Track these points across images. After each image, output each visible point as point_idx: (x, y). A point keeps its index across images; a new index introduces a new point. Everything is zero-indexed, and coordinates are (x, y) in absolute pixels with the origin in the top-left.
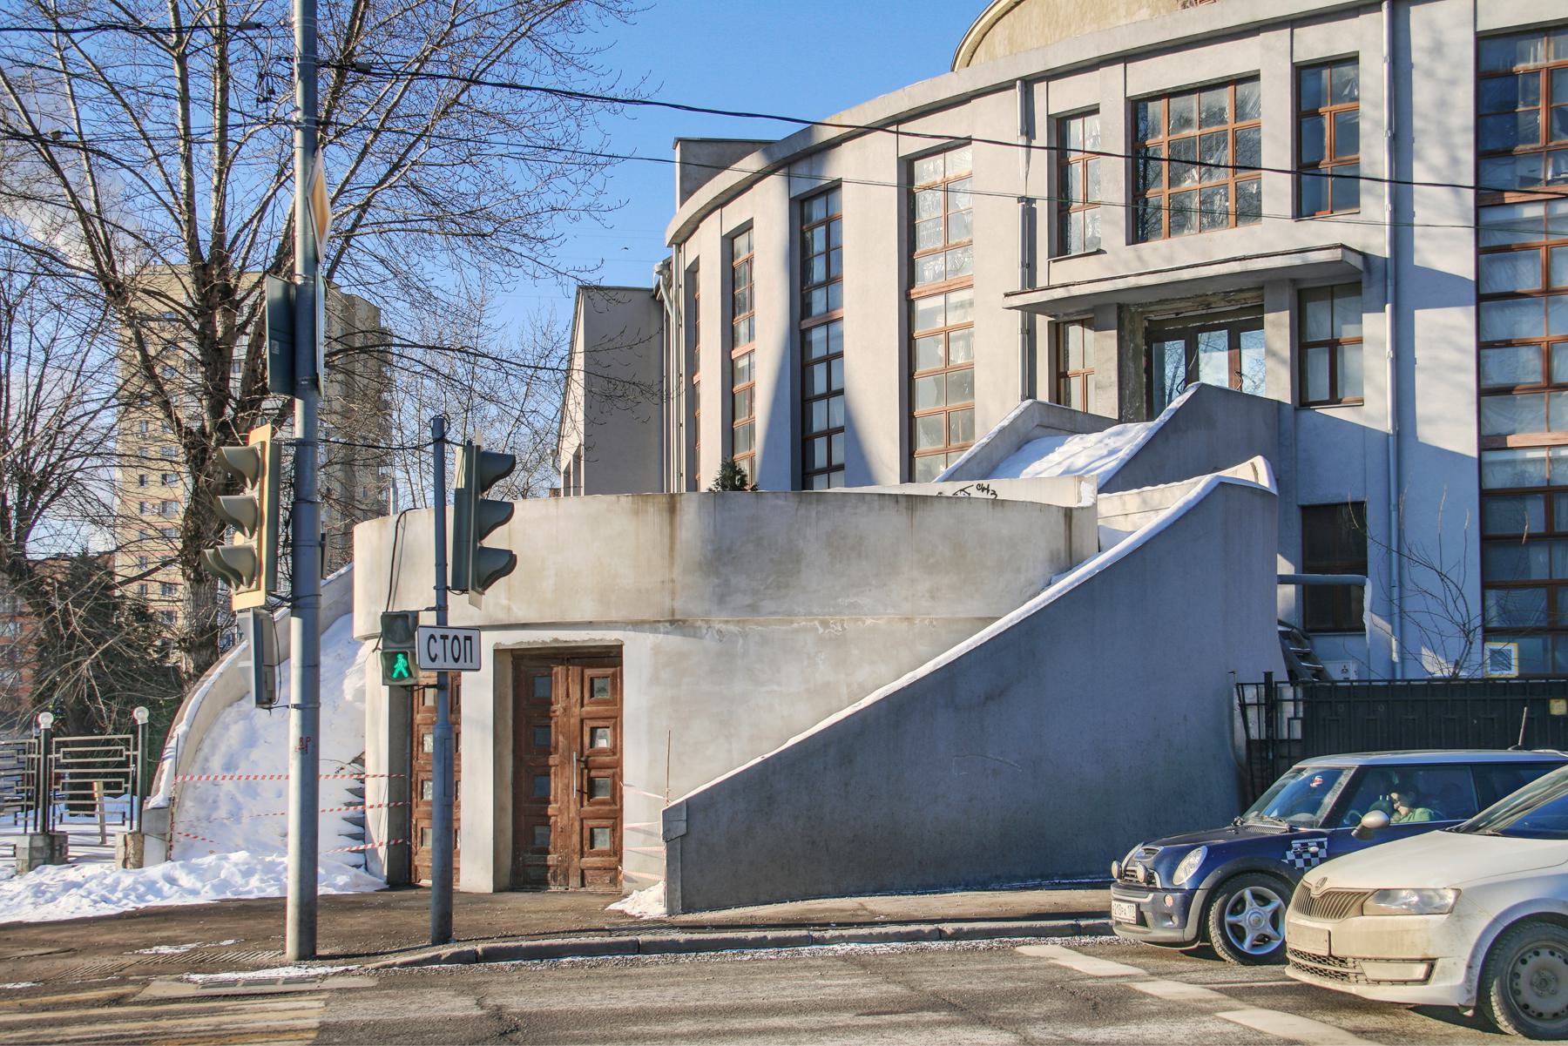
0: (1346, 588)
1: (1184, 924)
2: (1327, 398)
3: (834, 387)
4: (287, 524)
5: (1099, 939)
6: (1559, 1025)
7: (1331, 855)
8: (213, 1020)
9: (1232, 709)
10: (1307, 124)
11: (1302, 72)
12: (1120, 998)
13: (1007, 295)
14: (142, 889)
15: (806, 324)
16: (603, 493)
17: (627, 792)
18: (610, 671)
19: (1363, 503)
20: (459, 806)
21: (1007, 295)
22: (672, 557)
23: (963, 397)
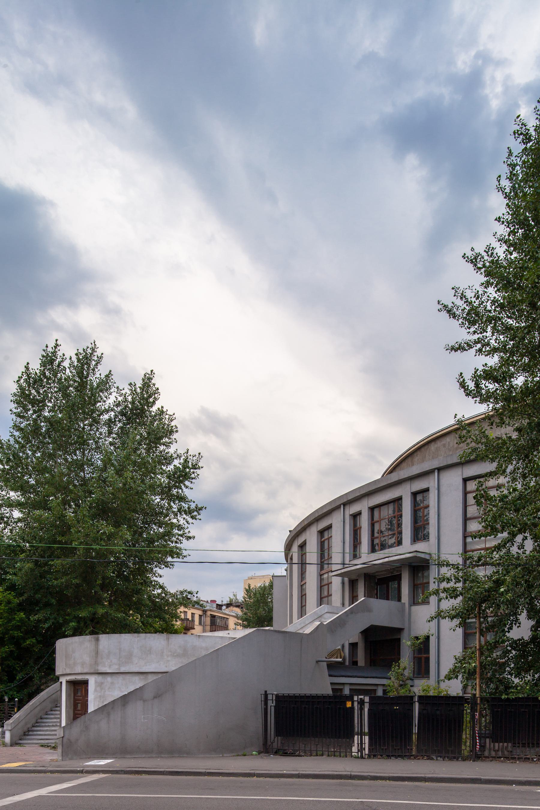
0: (459, 741)
3: (330, 594)
4: (470, 722)
5: (297, 773)
6: (539, 790)
7: (74, 635)
9: (27, 761)
10: (123, 772)
11: (415, 494)
14: (445, 563)
17: (68, 639)
18: (361, 662)
22: (391, 472)
23: (412, 704)
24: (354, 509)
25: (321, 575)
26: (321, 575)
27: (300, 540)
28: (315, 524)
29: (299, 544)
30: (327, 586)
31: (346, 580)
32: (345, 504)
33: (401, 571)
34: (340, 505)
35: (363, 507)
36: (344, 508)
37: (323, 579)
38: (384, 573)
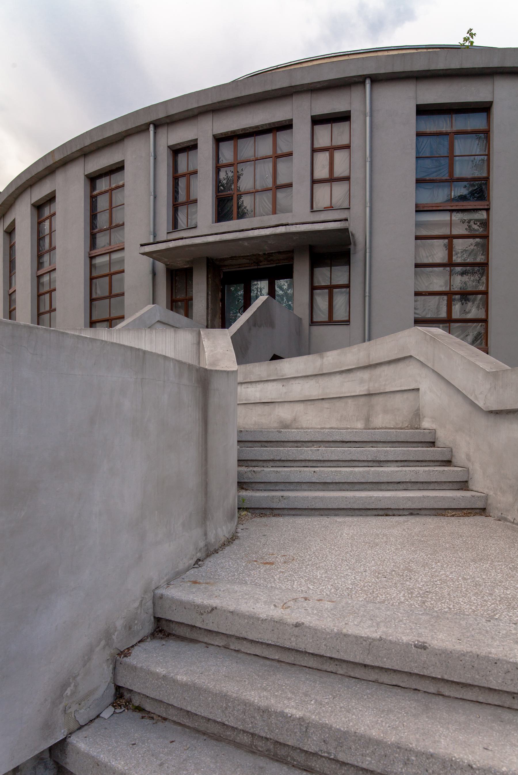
1: (485, 151)
2: (326, 319)
6: (517, 704)
8: (452, 205)
12: (295, 420)
13: (142, 245)
15: (94, 253)
16: (256, 362)
19: (274, 355)
20: (244, 129)
21: (142, 245)
24: (180, 135)
25: (92, 258)
26: (92, 258)
27: (39, 193)
28: (81, 161)
29: (34, 200)
30: (47, 296)
31: (161, 267)
32: (158, 125)
33: (292, 259)
34: (148, 125)
35: (204, 131)
36: (155, 133)
37: (43, 284)
38: (245, 261)
